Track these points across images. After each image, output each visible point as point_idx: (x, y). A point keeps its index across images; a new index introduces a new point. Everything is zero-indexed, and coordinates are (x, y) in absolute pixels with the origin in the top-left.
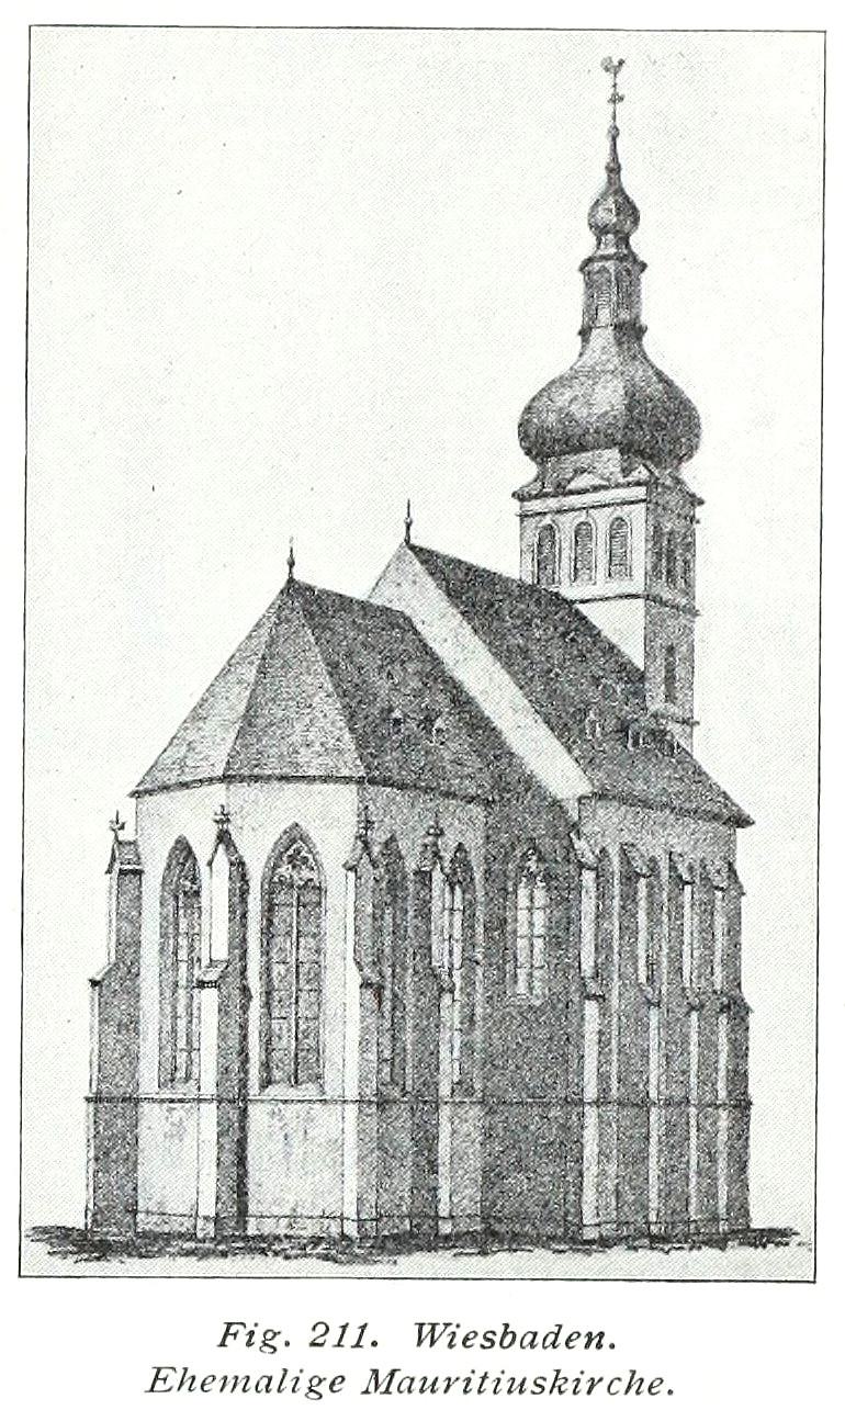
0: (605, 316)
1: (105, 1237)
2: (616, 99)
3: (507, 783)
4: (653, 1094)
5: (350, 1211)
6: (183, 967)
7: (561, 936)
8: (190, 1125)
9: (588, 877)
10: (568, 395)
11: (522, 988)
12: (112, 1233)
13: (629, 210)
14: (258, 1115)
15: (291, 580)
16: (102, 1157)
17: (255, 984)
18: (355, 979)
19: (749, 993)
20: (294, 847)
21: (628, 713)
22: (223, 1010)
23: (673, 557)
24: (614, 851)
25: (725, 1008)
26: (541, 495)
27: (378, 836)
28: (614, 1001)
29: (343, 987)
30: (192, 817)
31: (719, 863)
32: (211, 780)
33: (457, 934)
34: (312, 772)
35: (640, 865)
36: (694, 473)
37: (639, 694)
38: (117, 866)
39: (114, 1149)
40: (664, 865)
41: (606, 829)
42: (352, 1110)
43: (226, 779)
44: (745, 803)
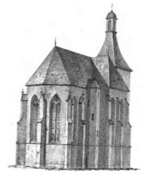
20: (56, 97)
30: (36, 91)
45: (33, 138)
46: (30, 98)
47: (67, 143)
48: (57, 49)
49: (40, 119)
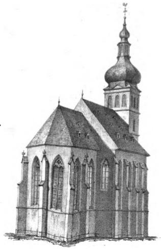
0: (122, 54)
1: (21, 234)
2: (125, 11)
3: (102, 147)
4: (129, 209)
5: (66, 236)
6: (36, 182)
7: (111, 177)
8: (37, 213)
9: (117, 166)
10: (115, 70)
11: (103, 188)
12: (22, 234)
13: (127, 33)
14: (50, 214)
15: (59, 105)
16: (19, 219)
17: (50, 186)
18: (69, 188)
19: (149, 189)
20: (58, 159)
21: (125, 133)
22: (44, 191)
23: (135, 103)
24: (122, 161)
25: (143, 192)
26: (109, 90)
27: (75, 158)
28: (122, 190)
29: (67, 188)
30: (38, 152)
31: (143, 164)
32: (42, 145)
33: (91, 176)
34: (62, 145)
35: (127, 164)
36: (139, 86)
37: (128, 130)
38: (23, 162)
39: (22, 219)
40: (132, 163)
41: (121, 157)
42: (67, 216)
43: (46, 145)
44: (148, 151)
45: (35, 202)
46: (31, 160)
47: (67, 212)
48: (60, 108)
49: (42, 181)
